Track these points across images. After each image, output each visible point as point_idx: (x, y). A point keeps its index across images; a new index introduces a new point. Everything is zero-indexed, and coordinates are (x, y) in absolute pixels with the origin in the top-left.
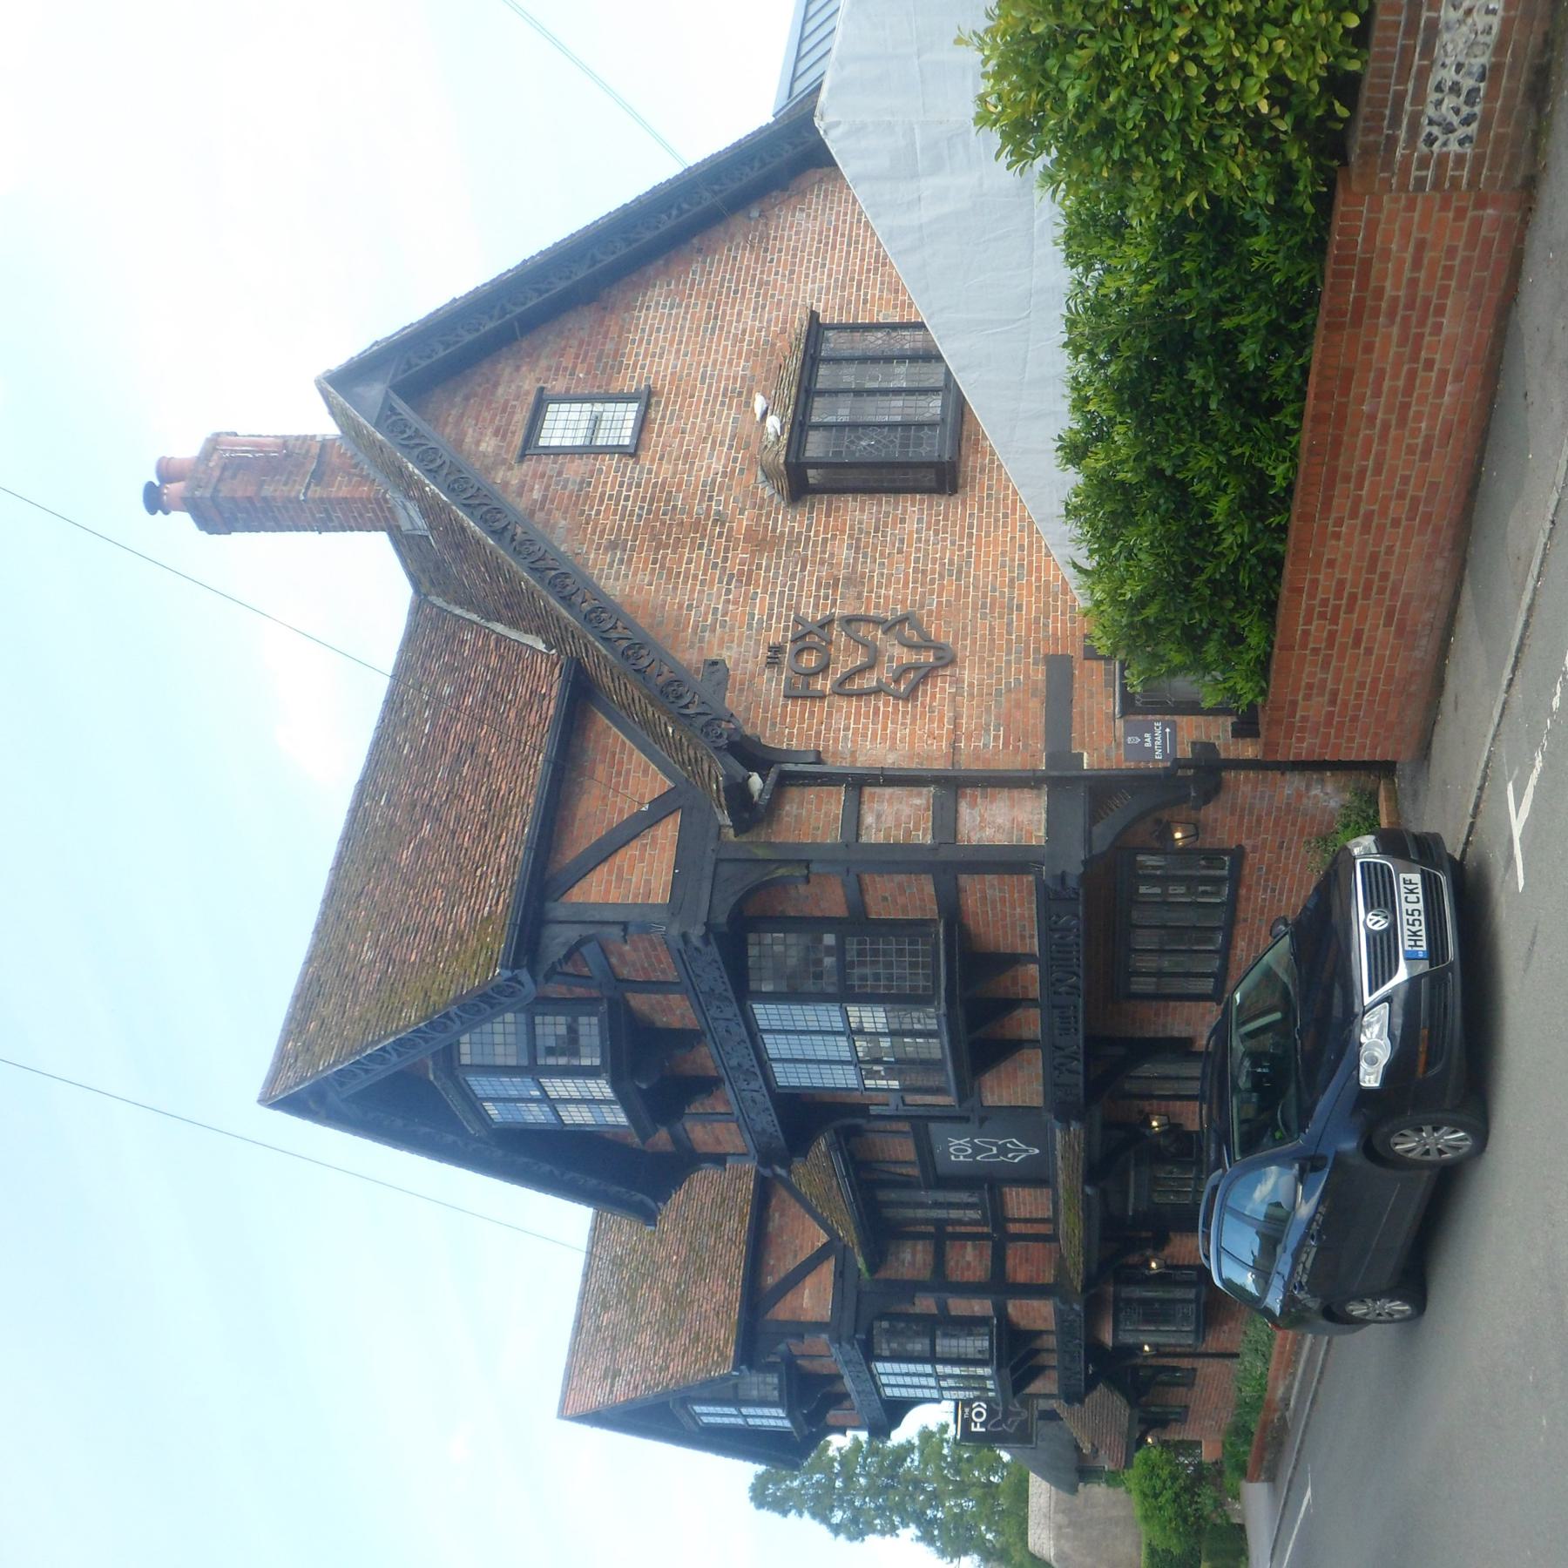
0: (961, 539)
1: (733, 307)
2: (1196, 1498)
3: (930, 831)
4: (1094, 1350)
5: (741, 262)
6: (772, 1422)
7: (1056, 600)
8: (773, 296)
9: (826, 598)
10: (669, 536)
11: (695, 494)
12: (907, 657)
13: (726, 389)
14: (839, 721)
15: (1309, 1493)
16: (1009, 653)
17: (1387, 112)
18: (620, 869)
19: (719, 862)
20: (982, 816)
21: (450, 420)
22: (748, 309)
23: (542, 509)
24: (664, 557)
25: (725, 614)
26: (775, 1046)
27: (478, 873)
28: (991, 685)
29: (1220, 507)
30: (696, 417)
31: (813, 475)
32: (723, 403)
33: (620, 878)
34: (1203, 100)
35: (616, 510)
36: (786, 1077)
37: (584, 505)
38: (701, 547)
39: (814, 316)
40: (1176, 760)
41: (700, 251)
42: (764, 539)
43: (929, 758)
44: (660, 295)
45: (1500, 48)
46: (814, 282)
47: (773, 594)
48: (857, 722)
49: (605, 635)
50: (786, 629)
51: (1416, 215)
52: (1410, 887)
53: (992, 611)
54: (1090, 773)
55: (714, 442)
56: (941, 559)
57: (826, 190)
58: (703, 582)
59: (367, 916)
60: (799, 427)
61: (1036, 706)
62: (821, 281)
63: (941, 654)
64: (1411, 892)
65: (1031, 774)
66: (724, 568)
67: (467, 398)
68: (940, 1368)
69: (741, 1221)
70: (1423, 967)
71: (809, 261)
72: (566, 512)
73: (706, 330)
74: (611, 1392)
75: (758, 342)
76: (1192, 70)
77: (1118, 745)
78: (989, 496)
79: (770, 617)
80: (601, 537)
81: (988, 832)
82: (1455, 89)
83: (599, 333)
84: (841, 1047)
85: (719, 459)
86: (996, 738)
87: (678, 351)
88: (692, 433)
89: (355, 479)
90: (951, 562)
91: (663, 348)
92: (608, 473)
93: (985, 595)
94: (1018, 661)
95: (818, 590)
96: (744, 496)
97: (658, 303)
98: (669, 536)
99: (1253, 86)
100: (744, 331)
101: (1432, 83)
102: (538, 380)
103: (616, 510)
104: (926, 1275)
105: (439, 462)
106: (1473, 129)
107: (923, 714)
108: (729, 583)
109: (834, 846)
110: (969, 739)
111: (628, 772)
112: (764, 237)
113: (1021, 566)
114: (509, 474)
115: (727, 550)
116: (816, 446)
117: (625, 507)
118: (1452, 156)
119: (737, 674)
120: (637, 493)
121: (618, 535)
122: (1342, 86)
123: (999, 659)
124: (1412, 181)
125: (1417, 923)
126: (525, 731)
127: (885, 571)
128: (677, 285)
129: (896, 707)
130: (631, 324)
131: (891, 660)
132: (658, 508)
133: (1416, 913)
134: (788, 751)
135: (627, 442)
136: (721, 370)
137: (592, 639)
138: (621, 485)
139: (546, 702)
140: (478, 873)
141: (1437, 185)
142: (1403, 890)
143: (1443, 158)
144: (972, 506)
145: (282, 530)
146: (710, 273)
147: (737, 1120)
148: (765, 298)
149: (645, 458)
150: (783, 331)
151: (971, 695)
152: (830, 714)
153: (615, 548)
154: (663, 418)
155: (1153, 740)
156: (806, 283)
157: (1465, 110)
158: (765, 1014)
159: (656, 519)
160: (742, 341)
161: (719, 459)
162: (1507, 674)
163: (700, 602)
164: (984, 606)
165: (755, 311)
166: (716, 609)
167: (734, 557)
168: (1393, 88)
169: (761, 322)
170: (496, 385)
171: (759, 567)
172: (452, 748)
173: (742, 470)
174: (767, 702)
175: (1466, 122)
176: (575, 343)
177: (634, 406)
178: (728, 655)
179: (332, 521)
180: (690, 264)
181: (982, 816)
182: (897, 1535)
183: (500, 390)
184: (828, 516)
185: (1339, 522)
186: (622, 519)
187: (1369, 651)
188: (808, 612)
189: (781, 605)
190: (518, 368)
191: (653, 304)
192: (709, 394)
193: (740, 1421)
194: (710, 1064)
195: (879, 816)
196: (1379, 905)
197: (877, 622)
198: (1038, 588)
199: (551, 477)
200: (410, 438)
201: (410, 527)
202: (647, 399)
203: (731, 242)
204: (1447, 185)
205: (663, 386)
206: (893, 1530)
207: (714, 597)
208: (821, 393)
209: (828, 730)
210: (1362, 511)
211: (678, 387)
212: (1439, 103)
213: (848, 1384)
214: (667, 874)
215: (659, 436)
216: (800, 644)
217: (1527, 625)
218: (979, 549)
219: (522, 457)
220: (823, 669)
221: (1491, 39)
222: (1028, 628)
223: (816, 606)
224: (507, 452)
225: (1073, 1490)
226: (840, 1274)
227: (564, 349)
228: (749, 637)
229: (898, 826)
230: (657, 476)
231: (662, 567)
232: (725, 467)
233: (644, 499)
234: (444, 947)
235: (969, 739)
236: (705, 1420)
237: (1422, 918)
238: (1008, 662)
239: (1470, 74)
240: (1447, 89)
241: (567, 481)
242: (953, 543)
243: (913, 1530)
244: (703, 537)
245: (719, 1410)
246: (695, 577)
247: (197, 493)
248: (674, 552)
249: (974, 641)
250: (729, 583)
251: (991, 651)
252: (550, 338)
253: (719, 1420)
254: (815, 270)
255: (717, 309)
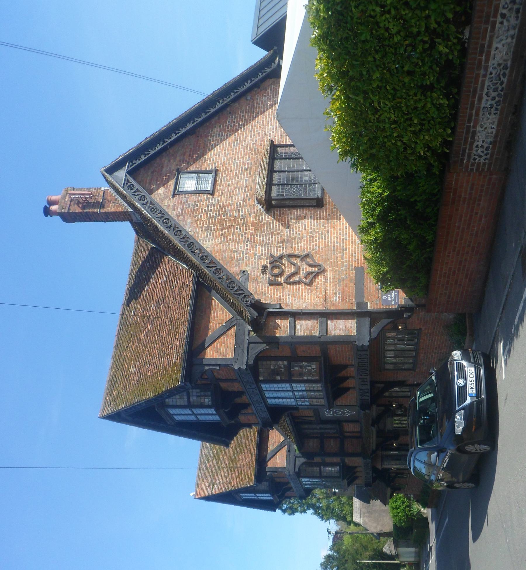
0: (326, 224)
1: (243, 136)
2: (411, 509)
3: (318, 331)
4: (375, 469)
5: (245, 118)
6: (267, 498)
7: (358, 247)
8: (257, 131)
9: (280, 247)
10: (226, 225)
11: (234, 208)
12: (310, 269)
13: (242, 168)
14: (286, 292)
15: (447, 520)
16: (343, 267)
17: (461, 153)
18: (217, 346)
19: (249, 343)
20: (335, 325)
21: (147, 181)
22: (248, 136)
23: (182, 215)
24: (225, 233)
25: (246, 254)
26: (267, 394)
27: (170, 347)
28: (337, 278)
29: (411, 247)
30: (232, 179)
31: (274, 202)
32: (241, 174)
33: (217, 349)
34: (403, 150)
35: (207, 215)
36: (271, 402)
37: (196, 213)
38: (237, 229)
39: (272, 142)
40: (399, 305)
41: (230, 113)
42: (258, 226)
43: (317, 305)
44: (217, 131)
45: (496, 136)
46: (271, 125)
47: (262, 246)
48: (293, 292)
49: (208, 266)
50: (267, 259)
51: (471, 178)
52: (471, 372)
53: (337, 252)
54: (370, 310)
55: (239, 188)
56: (319, 232)
57: (274, 88)
58: (238, 242)
59: (131, 355)
60: (269, 185)
61: (352, 285)
62: (274, 125)
63: (320, 268)
64: (471, 374)
65: (351, 311)
66: (245, 237)
67: (152, 172)
68: (294, 385)
69: (254, 434)
70: (475, 399)
71: (269, 117)
72: (190, 216)
73: (234, 145)
74: (212, 490)
75: (252, 149)
76: (399, 144)
77: (380, 299)
78: (334, 208)
79: (262, 255)
80: (203, 226)
81: (337, 331)
82: (482, 146)
83: (197, 146)
84: (290, 394)
85: (241, 195)
86: (339, 297)
87: (225, 153)
88: (231, 185)
89: (116, 205)
90: (322, 234)
91: (219, 152)
92: (204, 201)
93: (334, 246)
94: (346, 270)
95: (277, 244)
96: (251, 209)
97: (217, 134)
98: (226, 225)
99: (418, 147)
100: (247, 145)
101: (475, 145)
102: (177, 165)
103: (207, 215)
104: (186, 404)
105: (146, 201)
106: (488, 156)
107: (315, 289)
108: (247, 242)
109: (287, 337)
110: (330, 298)
111: (217, 311)
112: (253, 107)
113: (346, 234)
114: (169, 202)
115: (246, 230)
116: (275, 192)
117: (210, 214)
118: (482, 163)
119: (252, 276)
120: (214, 209)
121: (209, 225)
122: (446, 143)
123: (339, 269)
124: (469, 169)
125: (473, 384)
126: (182, 297)
127: (300, 237)
128: (223, 127)
129: (306, 288)
130: (208, 143)
131: (303, 270)
132: (222, 214)
133: (473, 381)
134: (270, 304)
135: (209, 189)
136: (240, 160)
137: (203, 268)
138: (208, 206)
139: (188, 288)
140: (170, 347)
141: (477, 170)
142: (469, 373)
143: (479, 164)
144: (329, 212)
145: (92, 221)
146: (234, 122)
147: (256, 415)
148: (254, 132)
149: (216, 194)
150: (261, 145)
151: (330, 282)
152: (283, 290)
153: (208, 230)
154: (221, 180)
155: (391, 298)
156: (268, 126)
157: (485, 152)
158: (264, 386)
159: (221, 218)
160: (247, 149)
161: (241, 195)
162: (501, 310)
163: (238, 249)
164: (334, 250)
165: (251, 137)
166: (243, 252)
167: (249, 232)
168: (462, 147)
169: (253, 141)
170: (162, 167)
171: (257, 236)
172: (156, 298)
173: (249, 199)
174: (262, 286)
175: (486, 155)
176: (188, 150)
177: (211, 175)
178: (248, 269)
179: (109, 218)
180: (227, 118)
181: (335, 325)
182: (306, 513)
183: (164, 169)
184: (280, 216)
185: (449, 253)
186: (209, 219)
187: (460, 285)
188: (275, 253)
189: (265, 250)
190: (169, 161)
191: (215, 135)
192: (236, 170)
193: (256, 498)
194: (247, 400)
195: (301, 326)
196: (461, 377)
197: (297, 256)
198: (352, 242)
199: (184, 203)
200: (135, 192)
201: (136, 220)
202: (216, 172)
203: (241, 109)
204: (480, 170)
205: (221, 167)
206: (304, 511)
207: (242, 248)
208: (276, 172)
209: (283, 295)
210: (456, 250)
211: (226, 168)
212: (477, 151)
213: (292, 485)
214: (232, 348)
215: (220, 187)
216: (272, 265)
217: (506, 299)
218: (331, 228)
219: (174, 196)
220: (281, 274)
221: (493, 135)
222: (349, 258)
223: (277, 250)
224: (168, 193)
225: (368, 502)
226: (289, 451)
227: (185, 153)
228: (255, 262)
229: (307, 329)
230: (220, 202)
231: (224, 236)
232: (244, 198)
233: (217, 210)
234: (160, 371)
235: (330, 298)
236: (244, 497)
237: (474, 383)
238: (342, 270)
239: (487, 143)
240: (479, 147)
241: (189, 204)
242: (323, 226)
243: (311, 511)
244: (237, 225)
245: (249, 495)
246: (236, 240)
247: (63, 211)
248: (228, 231)
249: (331, 263)
250: (247, 242)
251: (337, 266)
252: (180, 148)
253: (248, 498)
254: (271, 121)
255: (238, 136)
